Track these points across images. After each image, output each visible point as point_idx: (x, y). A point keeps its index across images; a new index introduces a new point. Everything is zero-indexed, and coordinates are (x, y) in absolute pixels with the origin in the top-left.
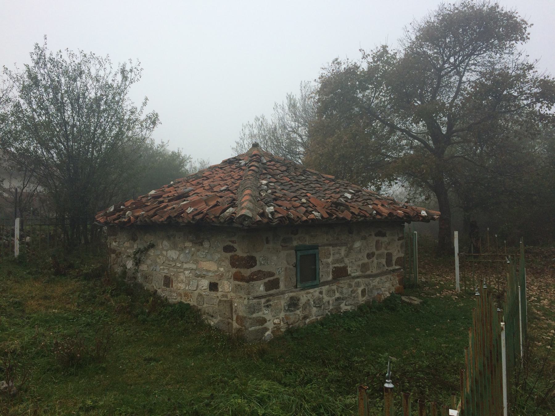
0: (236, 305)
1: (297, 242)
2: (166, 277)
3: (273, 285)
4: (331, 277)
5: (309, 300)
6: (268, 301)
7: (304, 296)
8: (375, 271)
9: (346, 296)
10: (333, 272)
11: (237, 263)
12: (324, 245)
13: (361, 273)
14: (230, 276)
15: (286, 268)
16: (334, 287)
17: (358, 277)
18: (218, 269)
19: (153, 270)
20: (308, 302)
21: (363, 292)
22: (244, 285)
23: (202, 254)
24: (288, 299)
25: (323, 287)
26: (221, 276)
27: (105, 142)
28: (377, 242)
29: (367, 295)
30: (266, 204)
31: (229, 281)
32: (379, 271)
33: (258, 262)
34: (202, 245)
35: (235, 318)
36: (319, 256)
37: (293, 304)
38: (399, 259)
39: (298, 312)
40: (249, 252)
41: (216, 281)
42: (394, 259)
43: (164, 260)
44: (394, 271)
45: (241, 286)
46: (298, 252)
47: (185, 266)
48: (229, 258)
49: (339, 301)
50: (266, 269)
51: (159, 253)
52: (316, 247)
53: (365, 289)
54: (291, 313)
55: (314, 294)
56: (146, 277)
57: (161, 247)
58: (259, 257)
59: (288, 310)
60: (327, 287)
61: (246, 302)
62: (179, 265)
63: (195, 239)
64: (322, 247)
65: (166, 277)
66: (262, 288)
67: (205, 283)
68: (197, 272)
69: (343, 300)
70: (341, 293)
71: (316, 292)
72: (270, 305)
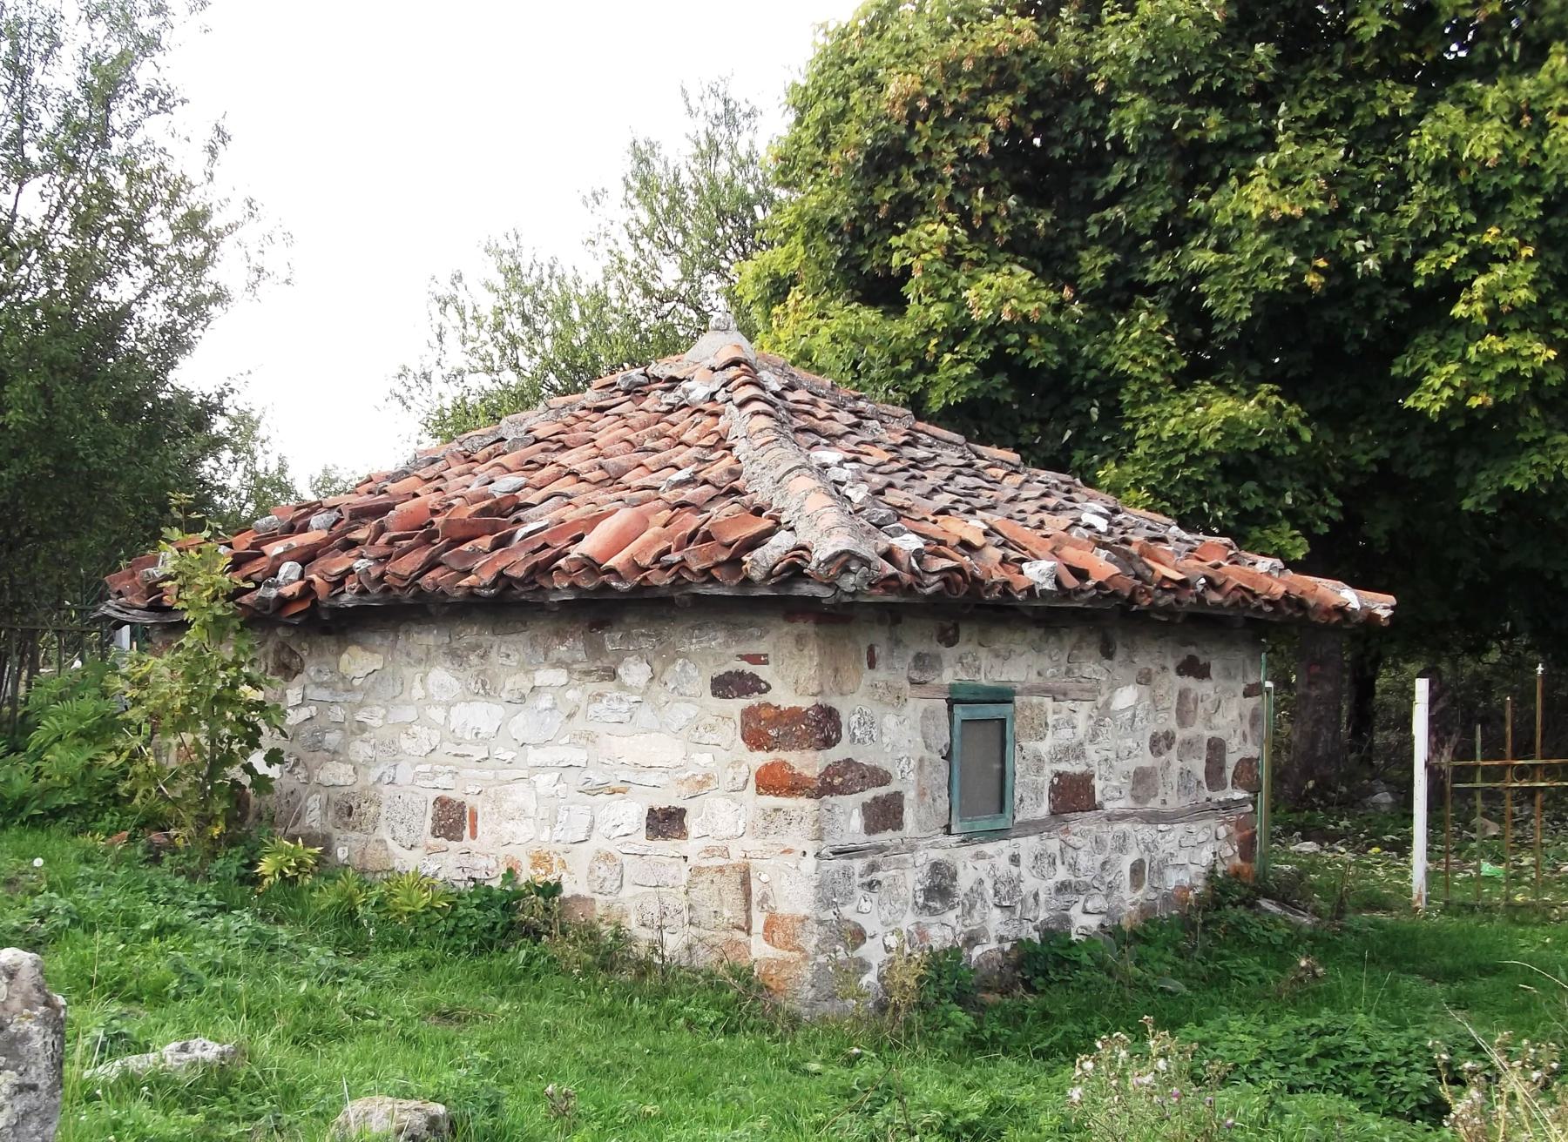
0: (764, 878)
1: (956, 673)
2: (442, 803)
3: (885, 814)
4: (1044, 810)
5: (981, 882)
6: (873, 868)
7: (969, 865)
8: (1175, 802)
9: (1088, 879)
10: (1053, 788)
11: (772, 733)
12: (1031, 691)
13: (1131, 804)
14: (741, 780)
15: (921, 760)
16: (1054, 845)
17: (1123, 817)
18: (687, 756)
19: (380, 779)
20: (976, 892)
21: (1137, 870)
22: (803, 809)
23: (614, 711)
24: (927, 868)
25: (1021, 841)
26: (703, 783)
27: (1232, 171)
28: (1183, 695)
29: (1146, 885)
30: (879, 526)
31: (734, 800)
32: (1185, 802)
33: (844, 731)
34: (612, 675)
35: (758, 924)
36: (1016, 728)
37: (939, 888)
38: (1247, 764)
39: (951, 916)
40: (821, 692)
41: (679, 804)
42: (1231, 761)
43: (435, 741)
44: (1227, 806)
45: (786, 813)
46: (957, 709)
47: (535, 756)
48: (737, 718)
49: (1067, 897)
50: (866, 756)
51: (409, 714)
52: (1003, 696)
53: (1141, 861)
54: (933, 919)
55: (997, 860)
56: (346, 811)
57: (418, 692)
58: (850, 709)
59: (925, 906)
60: (1034, 839)
61: (810, 863)
62: (508, 756)
63: (581, 656)
64: (1025, 699)
65: (442, 803)
66: (857, 821)
67: (632, 813)
68: (590, 773)
69: (1078, 892)
70: (1073, 867)
71: (999, 851)
72: (879, 883)
